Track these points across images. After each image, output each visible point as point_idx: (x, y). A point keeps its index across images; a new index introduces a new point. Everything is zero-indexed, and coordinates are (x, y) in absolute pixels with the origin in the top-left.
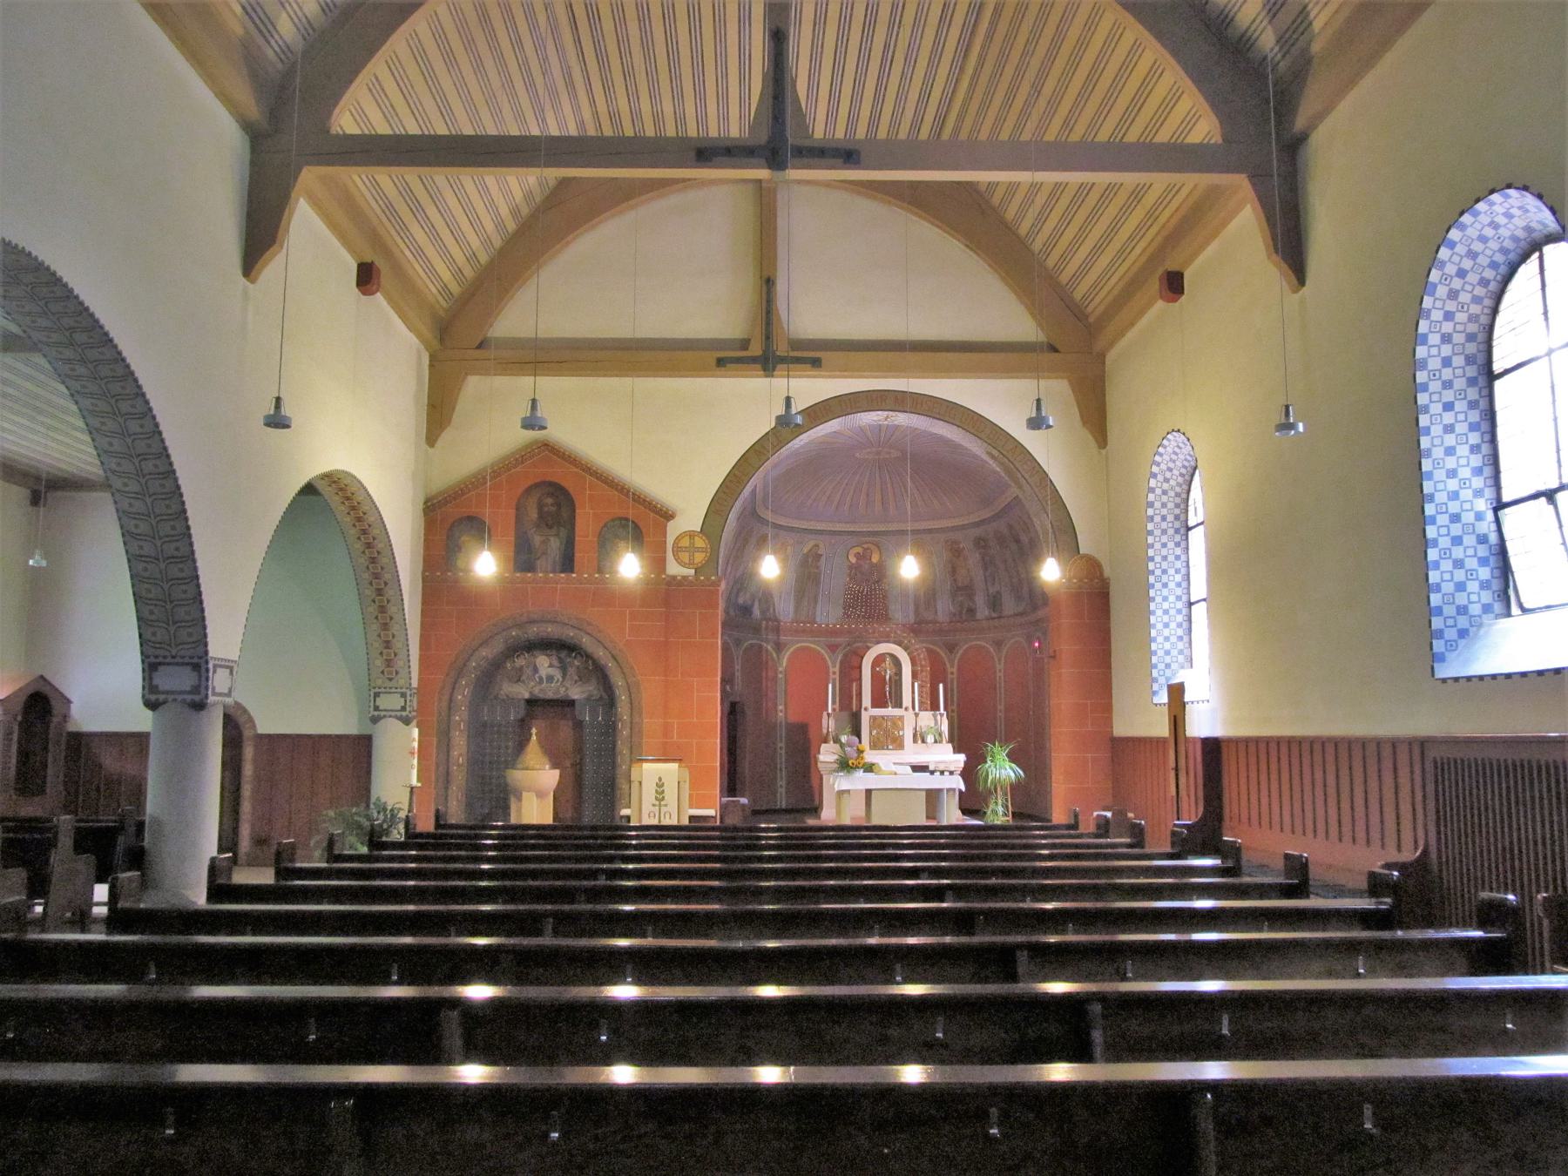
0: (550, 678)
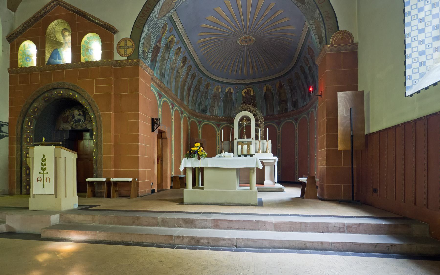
0: (79, 120)
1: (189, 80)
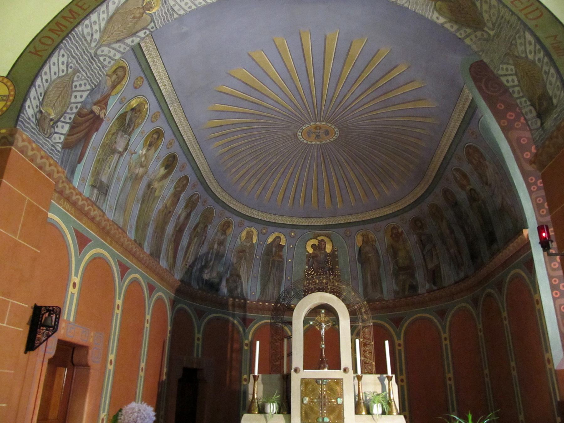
1: (180, 209)
